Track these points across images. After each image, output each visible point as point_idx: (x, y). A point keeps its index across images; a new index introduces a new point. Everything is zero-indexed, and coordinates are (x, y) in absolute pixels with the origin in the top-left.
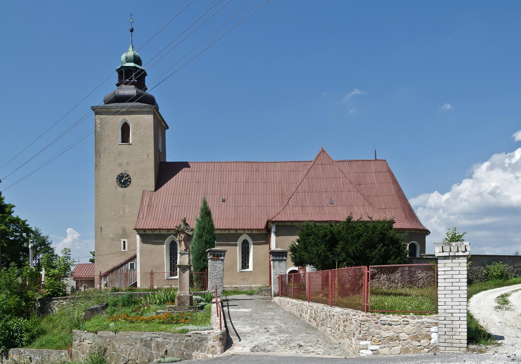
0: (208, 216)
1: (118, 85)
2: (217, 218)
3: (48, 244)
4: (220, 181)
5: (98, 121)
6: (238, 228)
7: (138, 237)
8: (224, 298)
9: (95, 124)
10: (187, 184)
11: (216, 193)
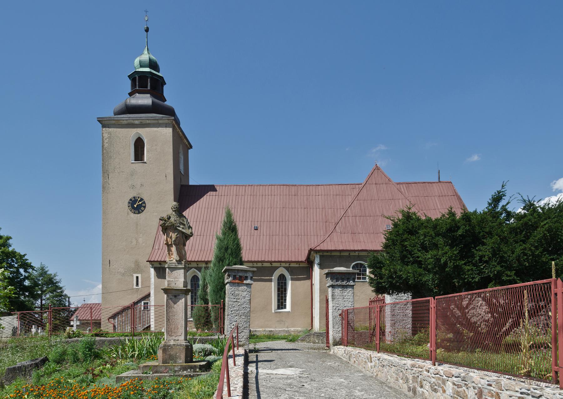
0: (232, 232)
1: (131, 94)
2: (248, 248)
3: (56, 283)
4: (251, 207)
5: (106, 135)
6: (273, 260)
7: (152, 271)
8: (251, 347)
9: (103, 139)
10: (212, 209)
11: (247, 220)
